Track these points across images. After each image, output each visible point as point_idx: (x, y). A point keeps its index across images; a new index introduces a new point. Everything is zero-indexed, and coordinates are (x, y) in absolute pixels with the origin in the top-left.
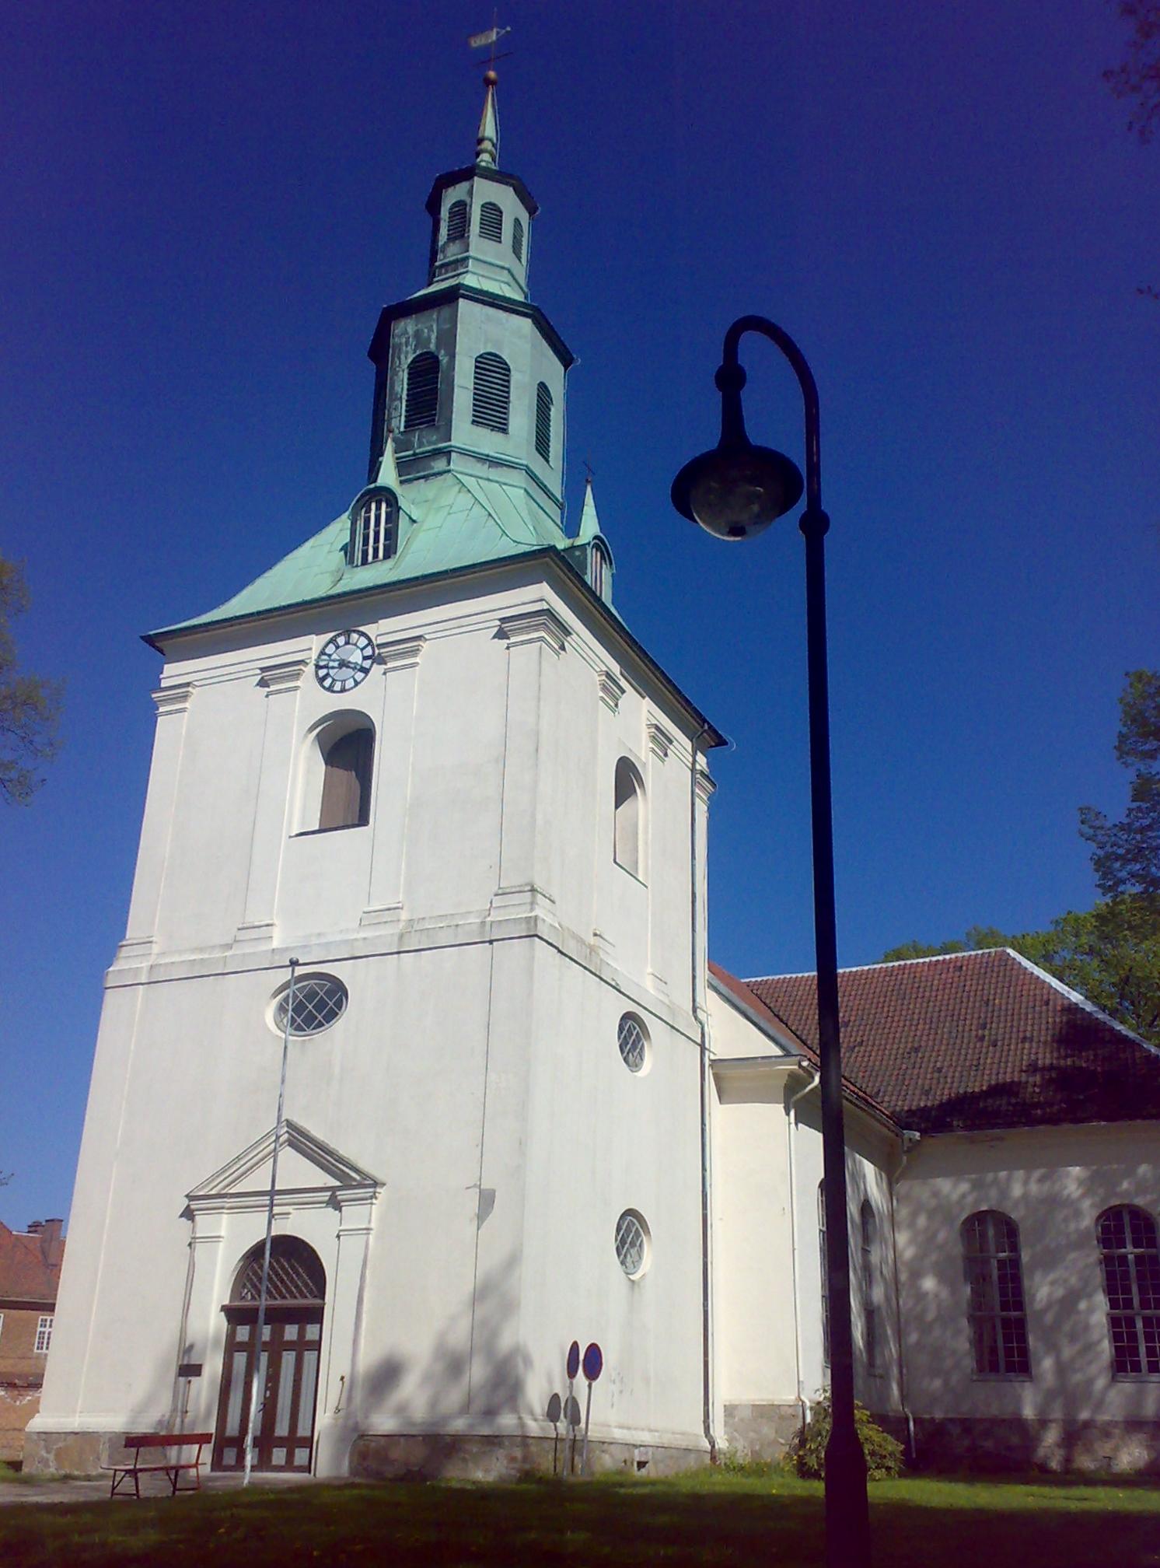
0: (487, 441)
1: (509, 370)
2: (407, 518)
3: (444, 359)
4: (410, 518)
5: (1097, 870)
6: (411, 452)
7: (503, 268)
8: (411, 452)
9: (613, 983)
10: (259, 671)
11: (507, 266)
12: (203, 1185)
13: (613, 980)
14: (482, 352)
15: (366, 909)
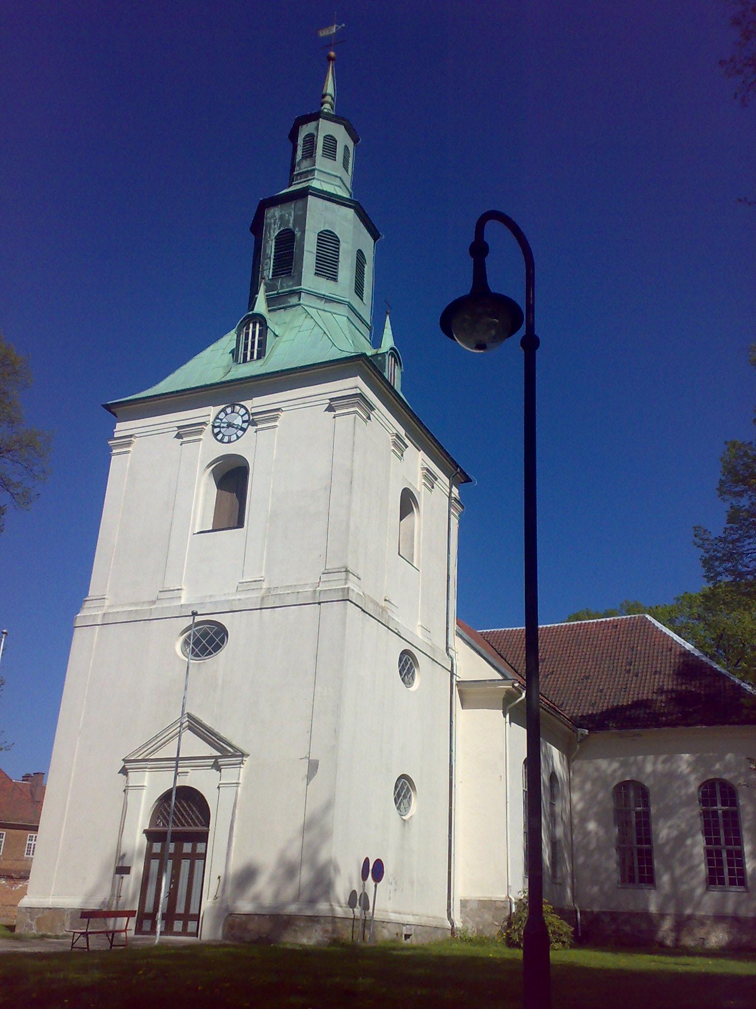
0: (324, 286)
1: (339, 242)
2: (273, 334)
3: (298, 234)
4: (274, 334)
5: (704, 567)
6: (276, 292)
7: (336, 176)
8: (276, 292)
9: (396, 631)
10: (176, 429)
11: (339, 175)
12: (134, 753)
13: (396, 629)
14: (322, 230)
15: (241, 581)
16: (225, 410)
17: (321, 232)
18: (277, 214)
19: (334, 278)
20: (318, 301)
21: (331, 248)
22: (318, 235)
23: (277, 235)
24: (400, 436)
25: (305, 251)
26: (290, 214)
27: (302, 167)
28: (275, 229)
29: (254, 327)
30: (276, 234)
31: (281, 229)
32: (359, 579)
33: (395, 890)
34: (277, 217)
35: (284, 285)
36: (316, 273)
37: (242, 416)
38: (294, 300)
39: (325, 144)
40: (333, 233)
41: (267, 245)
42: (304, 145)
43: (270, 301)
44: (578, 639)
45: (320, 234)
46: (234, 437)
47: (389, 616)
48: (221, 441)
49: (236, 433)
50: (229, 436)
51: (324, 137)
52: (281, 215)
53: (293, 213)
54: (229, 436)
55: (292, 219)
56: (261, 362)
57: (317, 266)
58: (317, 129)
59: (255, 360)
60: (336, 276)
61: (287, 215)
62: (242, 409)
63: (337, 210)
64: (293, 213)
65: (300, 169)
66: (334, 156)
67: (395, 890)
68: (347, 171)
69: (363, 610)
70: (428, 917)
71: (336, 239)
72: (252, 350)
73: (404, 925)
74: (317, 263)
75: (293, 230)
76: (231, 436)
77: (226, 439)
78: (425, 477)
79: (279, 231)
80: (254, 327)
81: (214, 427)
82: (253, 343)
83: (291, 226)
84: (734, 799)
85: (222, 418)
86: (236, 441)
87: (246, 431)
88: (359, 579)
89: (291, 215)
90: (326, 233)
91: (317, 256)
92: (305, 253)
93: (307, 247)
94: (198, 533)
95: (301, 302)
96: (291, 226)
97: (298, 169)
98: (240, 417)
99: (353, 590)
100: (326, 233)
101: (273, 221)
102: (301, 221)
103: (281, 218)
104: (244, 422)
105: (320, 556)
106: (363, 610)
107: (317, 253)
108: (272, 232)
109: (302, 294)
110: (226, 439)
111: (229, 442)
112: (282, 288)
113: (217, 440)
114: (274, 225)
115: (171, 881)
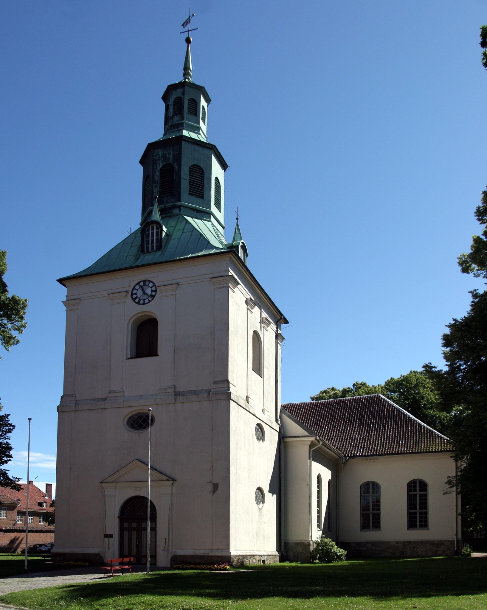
3: (177, 167)
9: (254, 414)
13: (254, 412)
16: (139, 284)
17: (192, 166)
18: (161, 153)
19: (201, 197)
20: (192, 212)
21: (198, 176)
22: (190, 168)
23: (162, 168)
24: (259, 295)
25: (182, 179)
26: (170, 154)
27: (175, 120)
28: (159, 163)
29: (153, 229)
30: (161, 166)
31: (164, 163)
32: (235, 386)
33: (257, 541)
34: (161, 155)
35: (169, 201)
37: (151, 288)
38: (176, 211)
39: (190, 103)
40: (200, 167)
41: (155, 174)
42: (174, 105)
43: (162, 212)
44: (446, 447)
45: (191, 167)
46: (147, 301)
47: (250, 406)
48: (138, 303)
49: (148, 298)
50: (143, 300)
51: (189, 100)
52: (164, 154)
53: (172, 152)
54: (143, 300)
55: (171, 157)
56: (159, 253)
57: (190, 189)
58: (183, 94)
59: (155, 251)
60: (202, 195)
61: (168, 154)
62: (151, 283)
63: (201, 151)
64: (172, 152)
65: (173, 122)
66: (195, 109)
67: (257, 541)
68: (205, 125)
69: (238, 404)
70: (271, 551)
71: (201, 170)
72: (153, 231)
73: (262, 556)
74: (190, 186)
75: (172, 164)
76: (144, 300)
77: (141, 302)
79: (163, 165)
80: (153, 229)
81: (132, 294)
82: (153, 240)
83: (171, 161)
84: (423, 491)
85: (138, 289)
86: (149, 304)
87: (155, 297)
88: (235, 386)
89: (171, 155)
90: (194, 166)
91: (190, 182)
92: (182, 181)
93: (183, 176)
95: (182, 212)
96: (171, 161)
97: (171, 121)
98: (150, 288)
99: (233, 394)
100: (194, 166)
101: (158, 158)
102: (178, 158)
103: (164, 155)
104: (152, 291)
105: (210, 374)
106: (238, 404)
107: (190, 180)
108: (158, 165)
109: (182, 208)
110: (141, 302)
111: (144, 304)
112: (167, 202)
113: (136, 302)
114: (159, 160)
115: (137, 541)
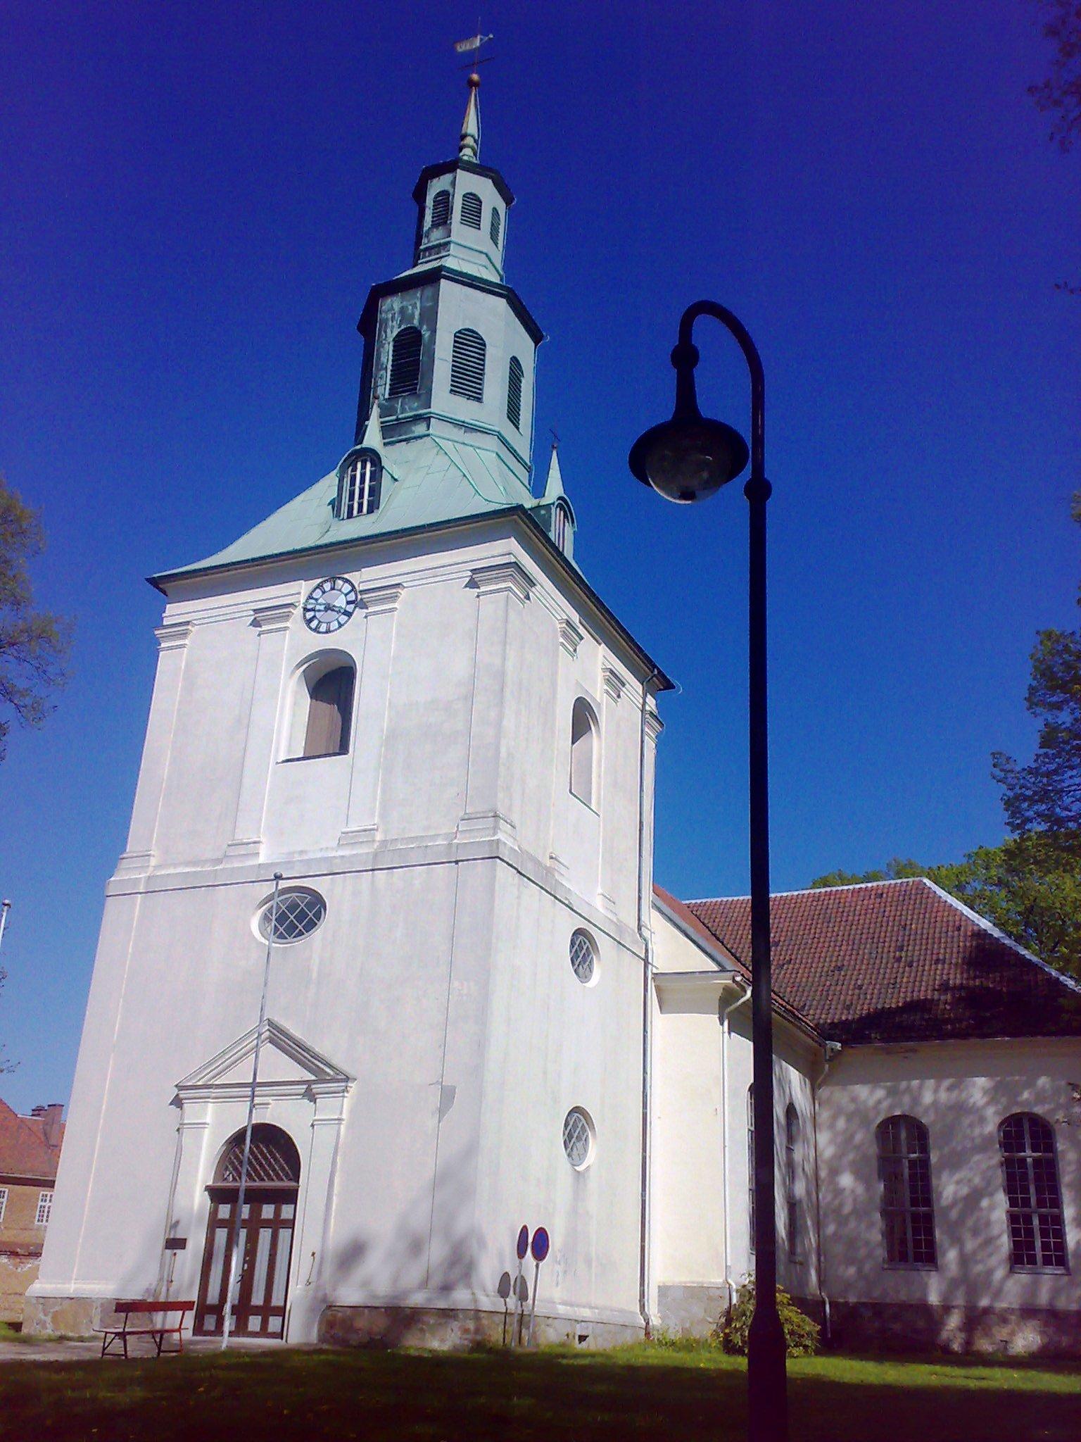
0: (463, 408)
1: (485, 345)
3: (426, 334)
4: (392, 477)
6: (394, 417)
7: (481, 252)
9: (567, 902)
11: (485, 251)
13: (566, 899)
14: (460, 328)
36: (452, 390)
78: (608, 681)
94: (284, 762)
